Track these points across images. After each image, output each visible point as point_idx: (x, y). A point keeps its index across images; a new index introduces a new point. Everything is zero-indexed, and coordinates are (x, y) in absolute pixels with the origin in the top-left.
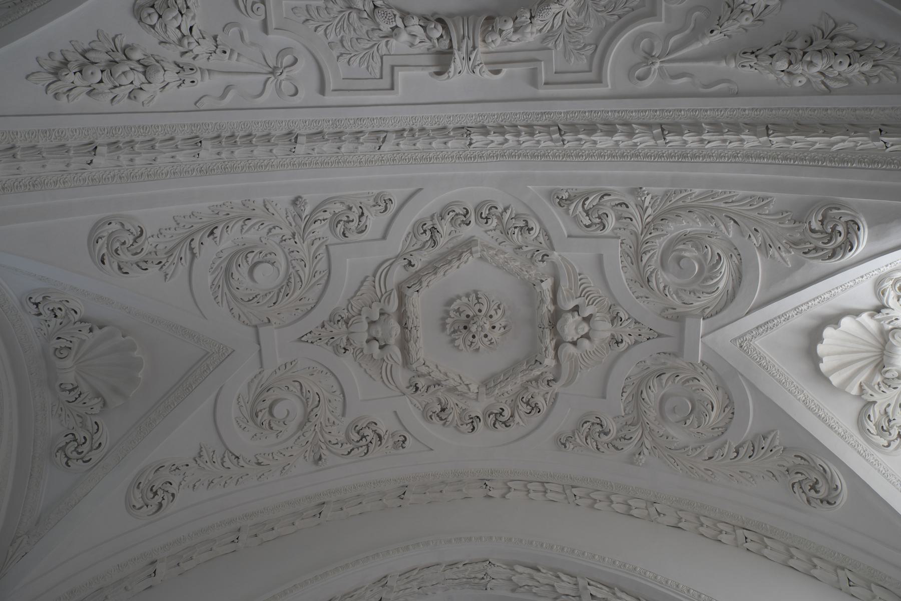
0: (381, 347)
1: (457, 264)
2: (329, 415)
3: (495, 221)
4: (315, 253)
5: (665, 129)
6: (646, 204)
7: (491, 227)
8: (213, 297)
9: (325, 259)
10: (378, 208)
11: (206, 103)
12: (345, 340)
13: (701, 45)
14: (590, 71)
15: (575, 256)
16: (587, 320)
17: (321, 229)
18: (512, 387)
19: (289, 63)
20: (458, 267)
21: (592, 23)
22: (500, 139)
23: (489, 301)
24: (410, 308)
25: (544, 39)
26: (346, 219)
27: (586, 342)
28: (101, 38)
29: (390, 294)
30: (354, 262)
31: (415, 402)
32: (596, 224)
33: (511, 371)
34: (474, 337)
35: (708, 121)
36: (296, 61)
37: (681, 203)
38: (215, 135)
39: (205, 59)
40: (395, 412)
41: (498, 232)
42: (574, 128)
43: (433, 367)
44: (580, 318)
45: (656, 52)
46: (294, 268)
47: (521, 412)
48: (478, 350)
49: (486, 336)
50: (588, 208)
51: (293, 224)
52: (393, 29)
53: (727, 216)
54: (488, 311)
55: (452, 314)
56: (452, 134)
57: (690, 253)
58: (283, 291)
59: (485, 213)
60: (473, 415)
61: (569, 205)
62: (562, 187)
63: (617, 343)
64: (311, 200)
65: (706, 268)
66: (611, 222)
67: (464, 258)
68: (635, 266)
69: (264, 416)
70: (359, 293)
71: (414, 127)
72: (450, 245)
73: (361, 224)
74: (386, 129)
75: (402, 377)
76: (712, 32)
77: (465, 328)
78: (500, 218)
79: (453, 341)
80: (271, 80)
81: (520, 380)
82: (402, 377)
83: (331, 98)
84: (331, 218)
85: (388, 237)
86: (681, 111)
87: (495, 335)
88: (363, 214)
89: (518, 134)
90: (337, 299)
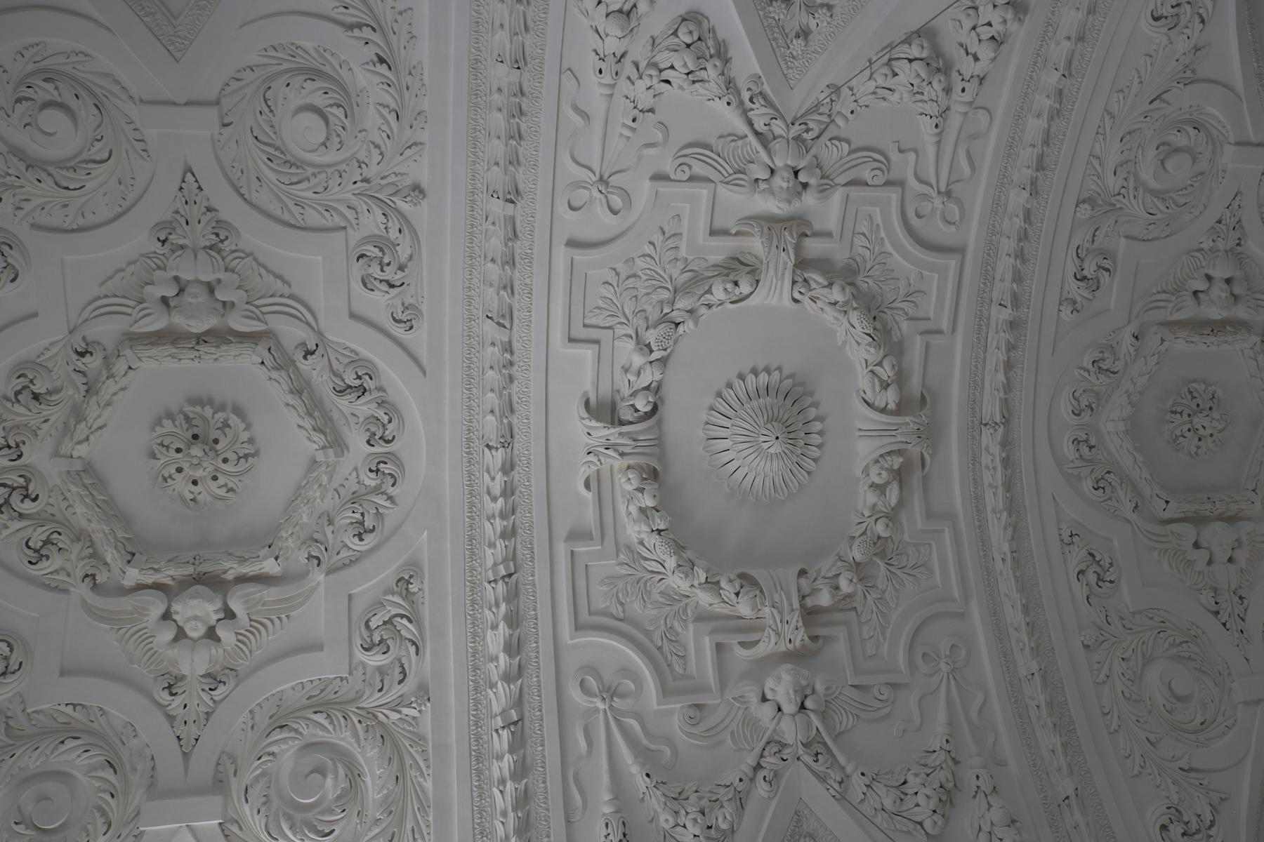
0: (165, 300)
1: (308, 426)
2: (37, 201)
3: (373, 483)
4: (335, 209)
5: (516, 726)
6: (405, 711)
7: (362, 477)
8: (275, 44)
9: (323, 223)
10: (400, 309)
11: (569, 84)
12: (180, 242)
13: (630, 762)
14: (590, 613)
15: (320, 607)
16: (211, 634)
17: (372, 222)
18: (81, 514)
19: (612, 203)
20: (299, 426)
21: (651, 612)
22: (497, 490)
23: (239, 474)
24: (234, 350)
25: (629, 548)
26: (386, 260)
27: (169, 635)
28: (1195, 394)
29: (259, 320)
30: (317, 271)
31: (54, 350)
32: (371, 637)
33: (112, 511)
34: (178, 450)
35: (531, 786)
36: (615, 213)
37: (408, 762)
38: (525, 88)
39: (627, 93)
40: (35, 315)
41: (355, 487)
42: (513, 595)
43: (123, 382)
44: (213, 623)
45: (617, 702)
46: (314, 175)
47: (30, 530)
48: (153, 456)
49: (179, 470)
50: (392, 625)
51: (383, 182)
52: (648, 346)
53: (394, 833)
54: (225, 473)
55: (220, 416)
56: (505, 421)
57: (331, 786)
58: (277, 153)
59: (385, 468)
60: (23, 448)
61: (400, 594)
62: (426, 581)
63: (170, 687)
64: (419, 213)
65: (309, 815)
66: (375, 660)
67: (316, 436)
68: (305, 702)
69: (46, 92)
70: (262, 271)
71: (516, 368)
72: (336, 415)
73: (377, 283)
74: (515, 328)
75: (106, 330)
76: (648, 775)
77: (195, 437)
78: (377, 490)
79: (170, 416)
80: (591, 175)
81: (98, 529)
82: (106, 330)
83: (561, 255)
84: (388, 239)
85: (353, 323)
86: (542, 745)
87: (181, 485)
88: (392, 286)
89: (503, 516)
90: (254, 235)
